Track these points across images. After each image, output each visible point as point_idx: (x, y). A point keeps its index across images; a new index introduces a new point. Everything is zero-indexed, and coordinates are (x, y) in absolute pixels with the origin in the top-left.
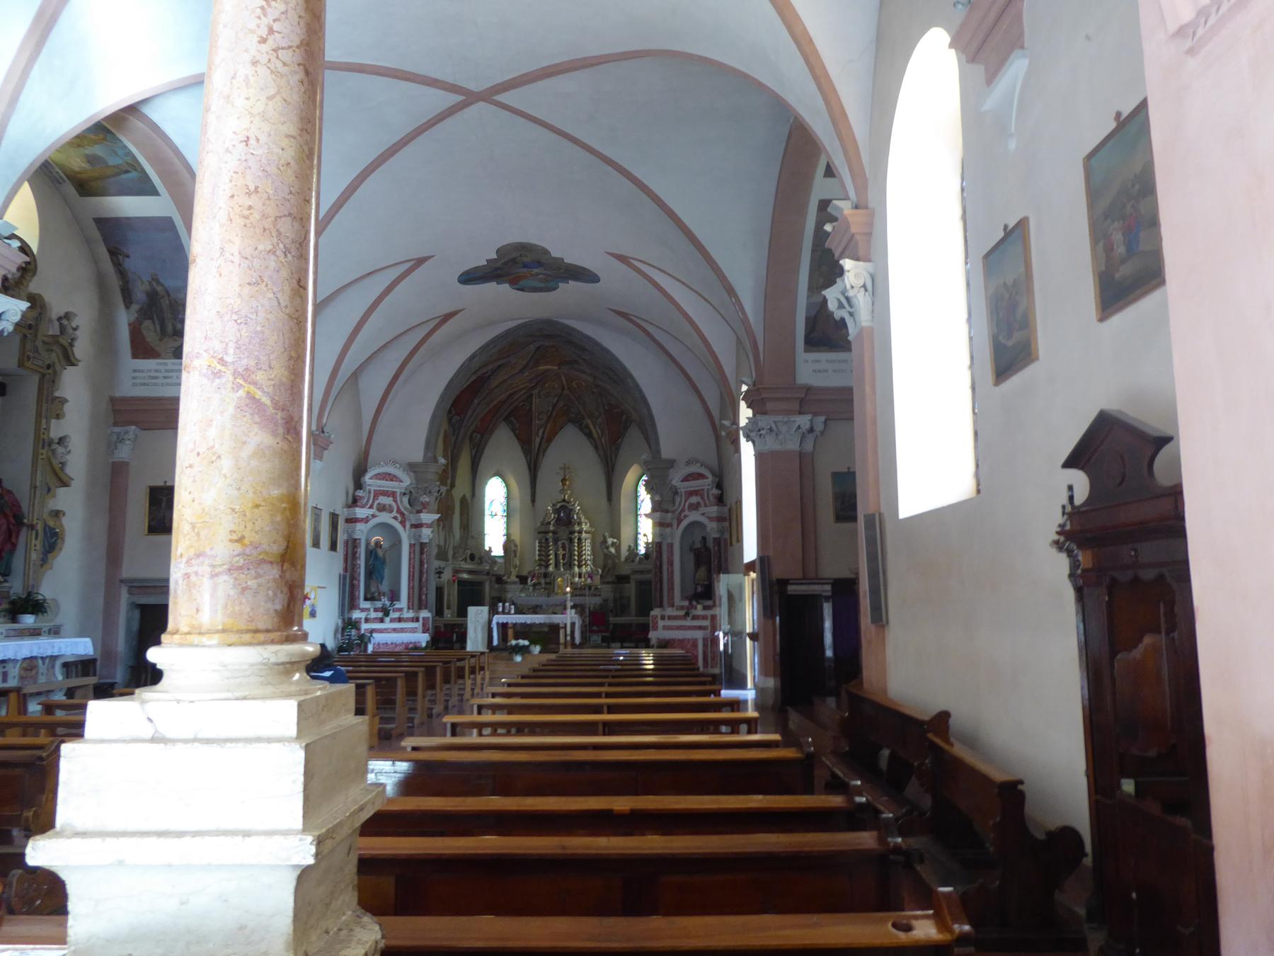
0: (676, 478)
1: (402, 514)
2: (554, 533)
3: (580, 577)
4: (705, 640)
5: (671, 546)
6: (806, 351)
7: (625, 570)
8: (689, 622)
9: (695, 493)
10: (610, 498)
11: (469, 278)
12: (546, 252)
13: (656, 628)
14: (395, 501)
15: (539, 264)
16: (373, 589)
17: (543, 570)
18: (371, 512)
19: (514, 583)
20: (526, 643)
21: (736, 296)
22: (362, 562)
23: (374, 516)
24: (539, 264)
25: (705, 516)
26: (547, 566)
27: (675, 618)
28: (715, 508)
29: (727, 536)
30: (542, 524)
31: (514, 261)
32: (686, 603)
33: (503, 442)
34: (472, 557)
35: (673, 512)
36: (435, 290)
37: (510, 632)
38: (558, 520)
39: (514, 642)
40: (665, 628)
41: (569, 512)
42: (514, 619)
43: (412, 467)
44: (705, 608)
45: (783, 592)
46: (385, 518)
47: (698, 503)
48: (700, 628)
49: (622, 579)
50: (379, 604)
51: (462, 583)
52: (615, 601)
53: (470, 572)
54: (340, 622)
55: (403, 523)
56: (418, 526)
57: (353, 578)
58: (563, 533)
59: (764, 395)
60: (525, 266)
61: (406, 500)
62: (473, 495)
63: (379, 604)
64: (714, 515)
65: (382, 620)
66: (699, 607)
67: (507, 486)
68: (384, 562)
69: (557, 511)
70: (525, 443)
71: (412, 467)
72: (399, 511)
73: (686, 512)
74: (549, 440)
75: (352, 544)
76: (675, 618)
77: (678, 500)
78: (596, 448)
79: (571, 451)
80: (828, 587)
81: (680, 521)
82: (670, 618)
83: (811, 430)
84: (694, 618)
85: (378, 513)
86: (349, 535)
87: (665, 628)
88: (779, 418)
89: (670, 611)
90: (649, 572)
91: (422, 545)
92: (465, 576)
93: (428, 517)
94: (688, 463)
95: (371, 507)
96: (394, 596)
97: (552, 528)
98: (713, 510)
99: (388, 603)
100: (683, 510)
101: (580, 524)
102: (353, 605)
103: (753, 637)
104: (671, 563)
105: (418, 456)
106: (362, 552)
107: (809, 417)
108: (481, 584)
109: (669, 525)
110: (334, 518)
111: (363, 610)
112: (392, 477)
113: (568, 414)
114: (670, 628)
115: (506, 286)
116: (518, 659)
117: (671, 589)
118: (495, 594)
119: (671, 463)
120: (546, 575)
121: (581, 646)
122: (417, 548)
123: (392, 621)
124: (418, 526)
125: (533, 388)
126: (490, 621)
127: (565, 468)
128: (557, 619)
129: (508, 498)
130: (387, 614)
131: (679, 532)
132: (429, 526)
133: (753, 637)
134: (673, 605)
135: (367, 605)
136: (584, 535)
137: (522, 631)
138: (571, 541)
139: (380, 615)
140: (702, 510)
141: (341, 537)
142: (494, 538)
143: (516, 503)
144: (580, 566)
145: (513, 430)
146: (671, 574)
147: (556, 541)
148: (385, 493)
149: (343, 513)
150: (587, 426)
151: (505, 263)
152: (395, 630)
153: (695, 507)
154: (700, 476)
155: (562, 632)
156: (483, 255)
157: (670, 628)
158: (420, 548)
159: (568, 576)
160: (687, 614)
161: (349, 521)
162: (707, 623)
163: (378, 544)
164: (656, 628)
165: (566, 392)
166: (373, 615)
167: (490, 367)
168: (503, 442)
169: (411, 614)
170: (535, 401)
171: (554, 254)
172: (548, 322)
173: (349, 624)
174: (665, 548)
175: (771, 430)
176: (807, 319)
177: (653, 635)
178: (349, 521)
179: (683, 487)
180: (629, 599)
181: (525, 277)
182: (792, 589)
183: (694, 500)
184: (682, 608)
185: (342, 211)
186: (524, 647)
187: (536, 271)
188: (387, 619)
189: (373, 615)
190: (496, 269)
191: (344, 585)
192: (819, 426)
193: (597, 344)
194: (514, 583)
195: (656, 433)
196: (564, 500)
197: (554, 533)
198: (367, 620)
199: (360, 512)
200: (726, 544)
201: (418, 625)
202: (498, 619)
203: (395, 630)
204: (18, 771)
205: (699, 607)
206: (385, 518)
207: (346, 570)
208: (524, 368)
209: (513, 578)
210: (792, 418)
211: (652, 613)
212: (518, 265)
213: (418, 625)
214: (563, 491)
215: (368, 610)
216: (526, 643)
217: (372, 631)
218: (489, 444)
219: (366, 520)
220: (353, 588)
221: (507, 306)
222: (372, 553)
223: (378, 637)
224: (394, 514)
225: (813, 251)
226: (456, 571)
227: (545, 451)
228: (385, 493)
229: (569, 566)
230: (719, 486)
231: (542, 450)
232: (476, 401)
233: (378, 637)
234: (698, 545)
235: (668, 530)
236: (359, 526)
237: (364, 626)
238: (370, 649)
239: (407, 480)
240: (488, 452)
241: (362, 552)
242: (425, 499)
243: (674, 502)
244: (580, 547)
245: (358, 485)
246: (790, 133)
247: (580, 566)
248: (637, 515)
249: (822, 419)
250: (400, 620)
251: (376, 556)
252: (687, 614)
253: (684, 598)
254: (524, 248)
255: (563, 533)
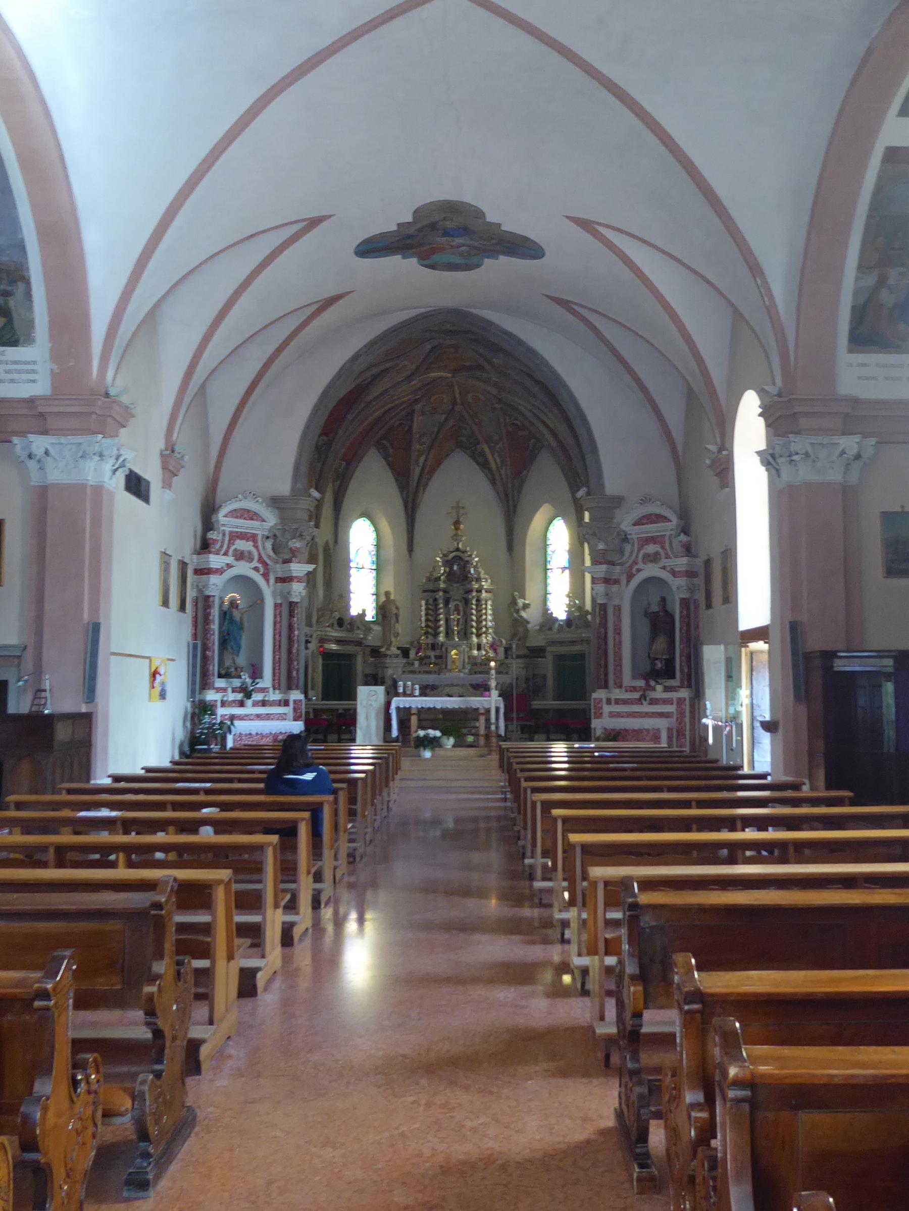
0: (625, 521)
1: (265, 564)
2: (445, 591)
3: (479, 648)
4: (669, 730)
5: (618, 609)
6: (850, 351)
7: (537, 641)
8: (645, 708)
9: (653, 540)
10: (510, 547)
11: (371, 248)
12: (479, 214)
13: (599, 715)
14: (256, 547)
15: (465, 231)
16: (228, 663)
17: (430, 640)
18: (230, 559)
19: (397, 656)
20: (438, 733)
21: (762, 274)
22: (215, 627)
23: (229, 566)
24: (465, 231)
25: (669, 572)
26: (436, 634)
27: (625, 702)
28: (685, 560)
29: (701, 597)
30: (429, 579)
31: (433, 226)
32: (641, 683)
33: (373, 475)
34: (340, 622)
35: (621, 564)
36: (323, 264)
37: (414, 720)
38: (450, 575)
39: (422, 733)
40: (612, 715)
41: (465, 564)
42: (418, 702)
43: (275, 502)
44: (667, 689)
45: (828, 669)
46: (243, 568)
47: (657, 554)
48: (661, 715)
49: (537, 652)
50: (237, 683)
51: (327, 656)
52: (527, 679)
53: (339, 641)
54: (189, 705)
55: (265, 576)
56: (285, 580)
57: (205, 648)
58: (457, 592)
59: (797, 409)
60: (447, 233)
61: (269, 545)
62: (336, 542)
63: (237, 683)
64: (683, 569)
65: (241, 704)
66: (659, 688)
67: (377, 530)
68: (241, 628)
69: (448, 563)
70: (401, 475)
71: (275, 502)
72: (260, 560)
73: (640, 565)
74: (432, 471)
75: (204, 602)
76: (625, 702)
77: (628, 548)
78: (493, 482)
79: (459, 485)
80: (890, 662)
81: (630, 577)
82: (617, 702)
83: (858, 457)
84: (653, 702)
85: (235, 563)
86: (200, 591)
87: (612, 715)
88: (819, 439)
89: (617, 694)
90: (588, 642)
91: (292, 605)
92: (334, 647)
93: (299, 569)
94: (644, 501)
95: (226, 554)
96: (256, 674)
97: (442, 585)
98: (681, 563)
99: (249, 681)
100: (636, 563)
101: (478, 580)
102: (205, 684)
103: (769, 726)
104: (618, 631)
105: (284, 487)
106: (215, 613)
107: (857, 438)
108: (350, 657)
109: (616, 582)
110: (183, 565)
111: (218, 690)
112: (250, 515)
113: (460, 438)
114: (619, 715)
115: (414, 260)
116: (427, 754)
117: (619, 664)
118: (369, 671)
119: (618, 501)
120: (434, 647)
121: (505, 739)
122: (285, 610)
123: (255, 704)
124: (285, 580)
125: (416, 401)
126: (388, 704)
127: (458, 507)
128: (476, 702)
129: (378, 546)
130: (248, 695)
131: (628, 591)
132: (299, 580)
133: (769, 726)
134: (620, 687)
135: (220, 683)
136: (484, 595)
137: (428, 717)
138: (467, 602)
139: (239, 696)
140: (664, 562)
141: (191, 594)
142: (362, 600)
143: (389, 553)
144: (479, 635)
145: (386, 458)
146: (618, 645)
147: (447, 602)
148: (243, 536)
149: (193, 561)
150: (482, 454)
151: (421, 230)
152: (259, 717)
153: (653, 558)
154: (665, 519)
155: (482, 719)
156: (393, 215)
157: (619, 715)
158: (288, 609)
159: (464, 647)
160: (644, 697)
161: (199, 572)
162: (671, 708)
163: (233, 603)
164: (599, 715)
165: (458, 408)
166: (232, 696)
167: (374, 371)
168: (373, 475)
169: (275, 696)
170: (417, 419)
171: (491, 218)
172: (456, 313)
173: (200, 710)
174: (610, 612)
175: (807, 455)
176: (854, 308)
177: (597, 725)
178: (199, 572)
179: (635, 532)
180: (544, 677)
181: (441, 249)
182: (840, 666)
183: (651, 549)
184: (634, 689)
185: (236, 143)
186: (435, 738)
187: (458, 241)
188: (249, 702)
189: (232, 696)
190: (409, 237)
191: (195, 656)
192: (868, 453)
193: (520, 342)
194: (397, 656)
195: (597, 461)
196: (458, 550)
197: (445, 591)
198: (223, 704)
199: (215, 561)
200: (697, 607)
201: (288, 710)
202: (396, 702)
203: (259, 717)
204: (113, 925)
205: (659, 688)
206: (243, 568)
207: (195, 636)
208: (413, 374)
209: (394, 650)
210: (836, 439)
211: (595, 695)
212: (442, 234)
213: (288, 710)
214: (456, 537)
215: (224, 690)
216: (438, 733)
217: (232, 718)
218: (356, 474)
219: (219, 571)
220: (205, 659)
221: (413, 287)
222: (225, 615)
223: (240, 727)
224: (255, 563)
225: (869, 217)
226: (323, 641)
227: (426, 485)
228: (243, 536)
229: (465, 634)
230: (685, 530)
231: (423, 482)
232: (350, 417)
233: (240, 727)
234: (655, 608)
235: (615, 588)
236: (214, 579)
237: (221, 711)
238: (230, 744)
239: (271, 519)
240: (354, 485)
241: (215, 613)
242: (296, 544)
243: (622, 552)
244: (479, 611)
245: (208, 524)
246: (869, 53)
247: (479, 635)
248: (546, 570)
249: (872, 441)
250: (264, 703)
251: (232, 619)
252: (644, 697)
253: (634, 677)
254: (452, 208)
255: (457, 592)
